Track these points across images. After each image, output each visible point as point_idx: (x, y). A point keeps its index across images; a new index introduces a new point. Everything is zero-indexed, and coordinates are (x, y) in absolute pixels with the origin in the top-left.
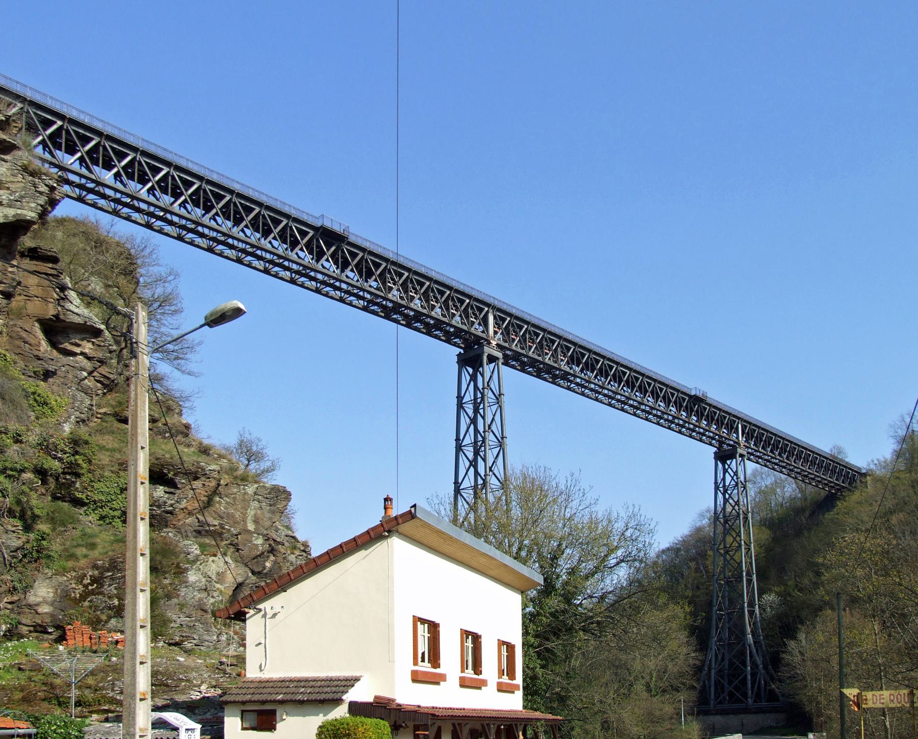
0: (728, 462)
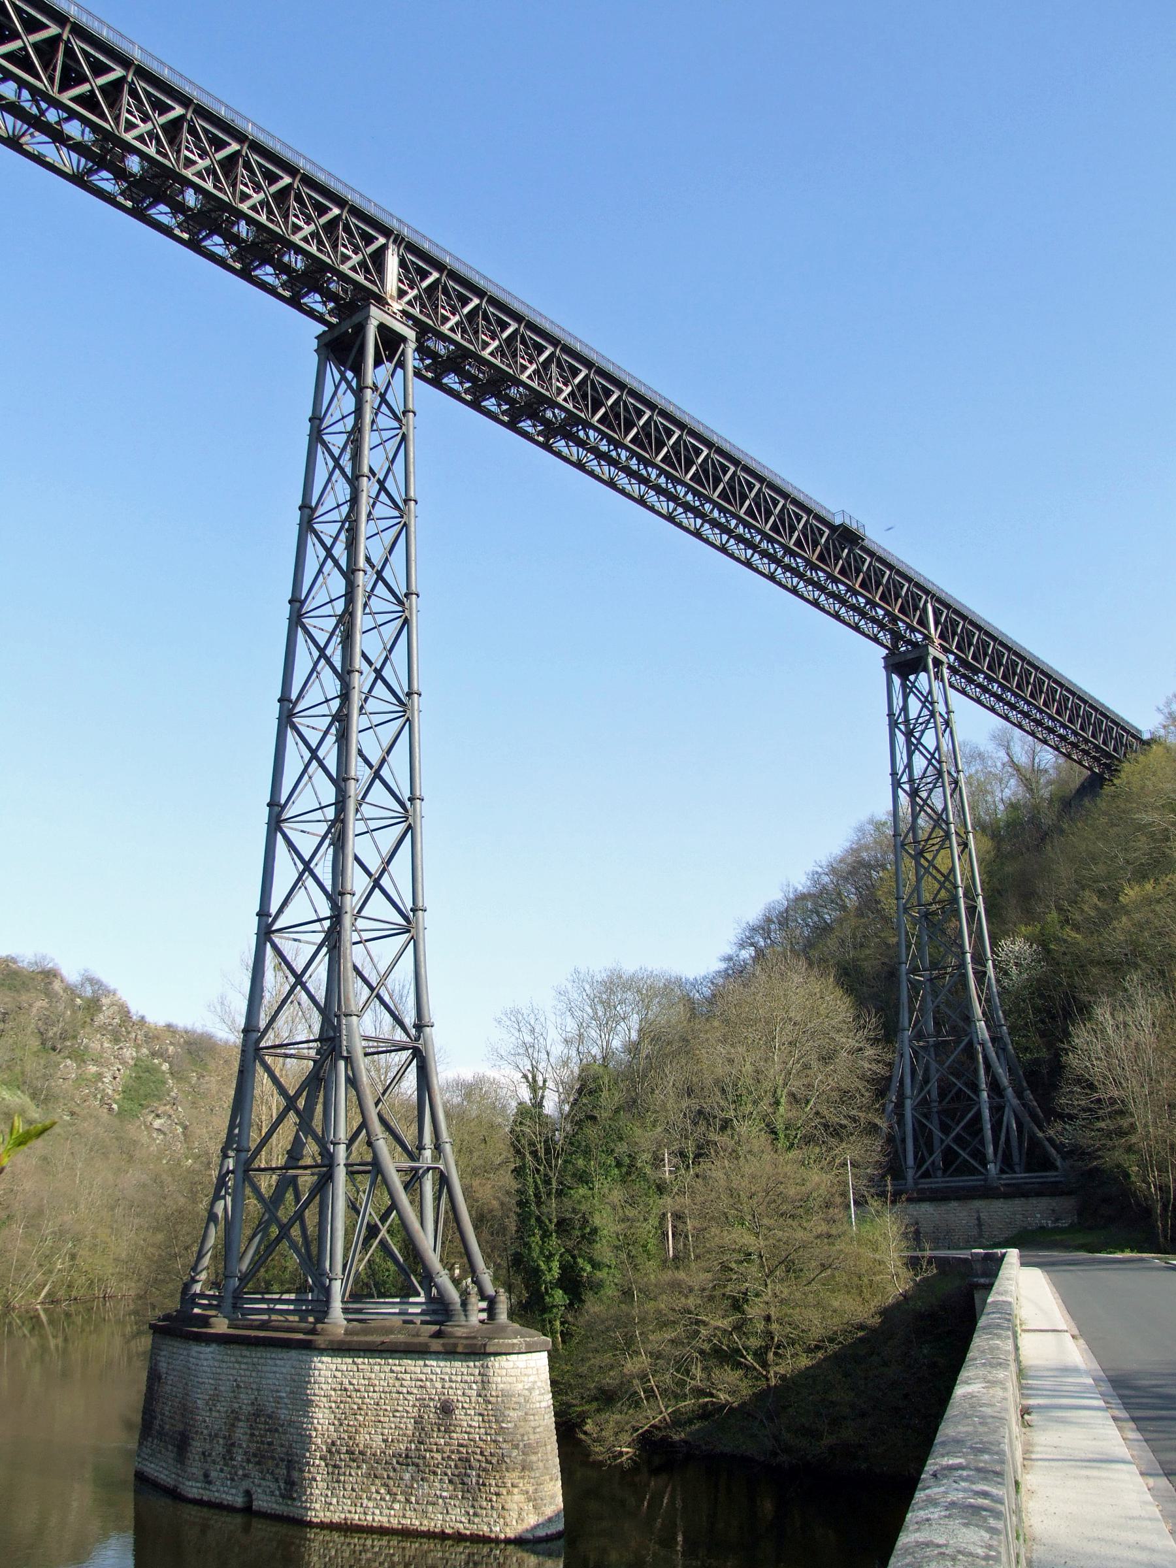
0: (912, 678)
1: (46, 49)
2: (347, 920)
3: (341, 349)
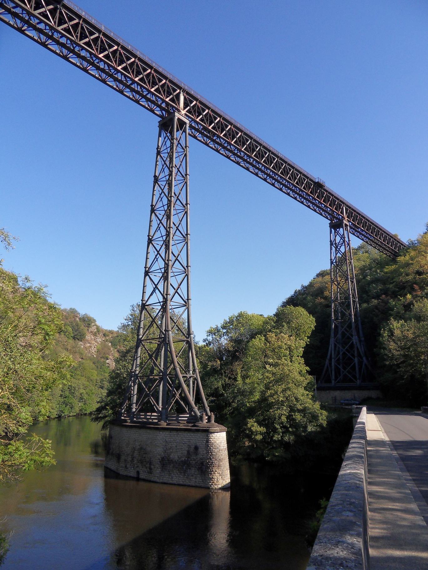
1: (75, 26)
2: (168, 302)
3: (166, 125)
